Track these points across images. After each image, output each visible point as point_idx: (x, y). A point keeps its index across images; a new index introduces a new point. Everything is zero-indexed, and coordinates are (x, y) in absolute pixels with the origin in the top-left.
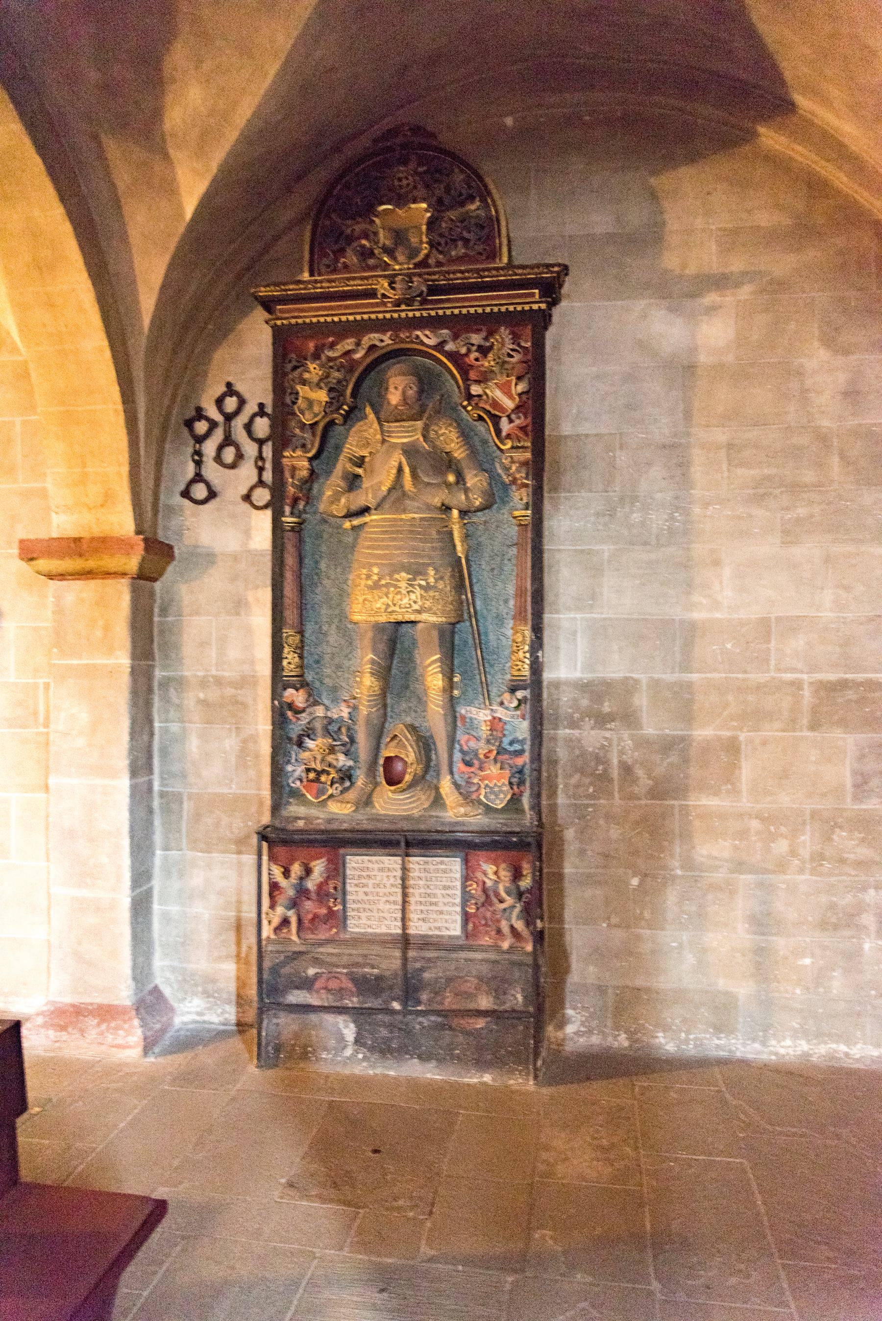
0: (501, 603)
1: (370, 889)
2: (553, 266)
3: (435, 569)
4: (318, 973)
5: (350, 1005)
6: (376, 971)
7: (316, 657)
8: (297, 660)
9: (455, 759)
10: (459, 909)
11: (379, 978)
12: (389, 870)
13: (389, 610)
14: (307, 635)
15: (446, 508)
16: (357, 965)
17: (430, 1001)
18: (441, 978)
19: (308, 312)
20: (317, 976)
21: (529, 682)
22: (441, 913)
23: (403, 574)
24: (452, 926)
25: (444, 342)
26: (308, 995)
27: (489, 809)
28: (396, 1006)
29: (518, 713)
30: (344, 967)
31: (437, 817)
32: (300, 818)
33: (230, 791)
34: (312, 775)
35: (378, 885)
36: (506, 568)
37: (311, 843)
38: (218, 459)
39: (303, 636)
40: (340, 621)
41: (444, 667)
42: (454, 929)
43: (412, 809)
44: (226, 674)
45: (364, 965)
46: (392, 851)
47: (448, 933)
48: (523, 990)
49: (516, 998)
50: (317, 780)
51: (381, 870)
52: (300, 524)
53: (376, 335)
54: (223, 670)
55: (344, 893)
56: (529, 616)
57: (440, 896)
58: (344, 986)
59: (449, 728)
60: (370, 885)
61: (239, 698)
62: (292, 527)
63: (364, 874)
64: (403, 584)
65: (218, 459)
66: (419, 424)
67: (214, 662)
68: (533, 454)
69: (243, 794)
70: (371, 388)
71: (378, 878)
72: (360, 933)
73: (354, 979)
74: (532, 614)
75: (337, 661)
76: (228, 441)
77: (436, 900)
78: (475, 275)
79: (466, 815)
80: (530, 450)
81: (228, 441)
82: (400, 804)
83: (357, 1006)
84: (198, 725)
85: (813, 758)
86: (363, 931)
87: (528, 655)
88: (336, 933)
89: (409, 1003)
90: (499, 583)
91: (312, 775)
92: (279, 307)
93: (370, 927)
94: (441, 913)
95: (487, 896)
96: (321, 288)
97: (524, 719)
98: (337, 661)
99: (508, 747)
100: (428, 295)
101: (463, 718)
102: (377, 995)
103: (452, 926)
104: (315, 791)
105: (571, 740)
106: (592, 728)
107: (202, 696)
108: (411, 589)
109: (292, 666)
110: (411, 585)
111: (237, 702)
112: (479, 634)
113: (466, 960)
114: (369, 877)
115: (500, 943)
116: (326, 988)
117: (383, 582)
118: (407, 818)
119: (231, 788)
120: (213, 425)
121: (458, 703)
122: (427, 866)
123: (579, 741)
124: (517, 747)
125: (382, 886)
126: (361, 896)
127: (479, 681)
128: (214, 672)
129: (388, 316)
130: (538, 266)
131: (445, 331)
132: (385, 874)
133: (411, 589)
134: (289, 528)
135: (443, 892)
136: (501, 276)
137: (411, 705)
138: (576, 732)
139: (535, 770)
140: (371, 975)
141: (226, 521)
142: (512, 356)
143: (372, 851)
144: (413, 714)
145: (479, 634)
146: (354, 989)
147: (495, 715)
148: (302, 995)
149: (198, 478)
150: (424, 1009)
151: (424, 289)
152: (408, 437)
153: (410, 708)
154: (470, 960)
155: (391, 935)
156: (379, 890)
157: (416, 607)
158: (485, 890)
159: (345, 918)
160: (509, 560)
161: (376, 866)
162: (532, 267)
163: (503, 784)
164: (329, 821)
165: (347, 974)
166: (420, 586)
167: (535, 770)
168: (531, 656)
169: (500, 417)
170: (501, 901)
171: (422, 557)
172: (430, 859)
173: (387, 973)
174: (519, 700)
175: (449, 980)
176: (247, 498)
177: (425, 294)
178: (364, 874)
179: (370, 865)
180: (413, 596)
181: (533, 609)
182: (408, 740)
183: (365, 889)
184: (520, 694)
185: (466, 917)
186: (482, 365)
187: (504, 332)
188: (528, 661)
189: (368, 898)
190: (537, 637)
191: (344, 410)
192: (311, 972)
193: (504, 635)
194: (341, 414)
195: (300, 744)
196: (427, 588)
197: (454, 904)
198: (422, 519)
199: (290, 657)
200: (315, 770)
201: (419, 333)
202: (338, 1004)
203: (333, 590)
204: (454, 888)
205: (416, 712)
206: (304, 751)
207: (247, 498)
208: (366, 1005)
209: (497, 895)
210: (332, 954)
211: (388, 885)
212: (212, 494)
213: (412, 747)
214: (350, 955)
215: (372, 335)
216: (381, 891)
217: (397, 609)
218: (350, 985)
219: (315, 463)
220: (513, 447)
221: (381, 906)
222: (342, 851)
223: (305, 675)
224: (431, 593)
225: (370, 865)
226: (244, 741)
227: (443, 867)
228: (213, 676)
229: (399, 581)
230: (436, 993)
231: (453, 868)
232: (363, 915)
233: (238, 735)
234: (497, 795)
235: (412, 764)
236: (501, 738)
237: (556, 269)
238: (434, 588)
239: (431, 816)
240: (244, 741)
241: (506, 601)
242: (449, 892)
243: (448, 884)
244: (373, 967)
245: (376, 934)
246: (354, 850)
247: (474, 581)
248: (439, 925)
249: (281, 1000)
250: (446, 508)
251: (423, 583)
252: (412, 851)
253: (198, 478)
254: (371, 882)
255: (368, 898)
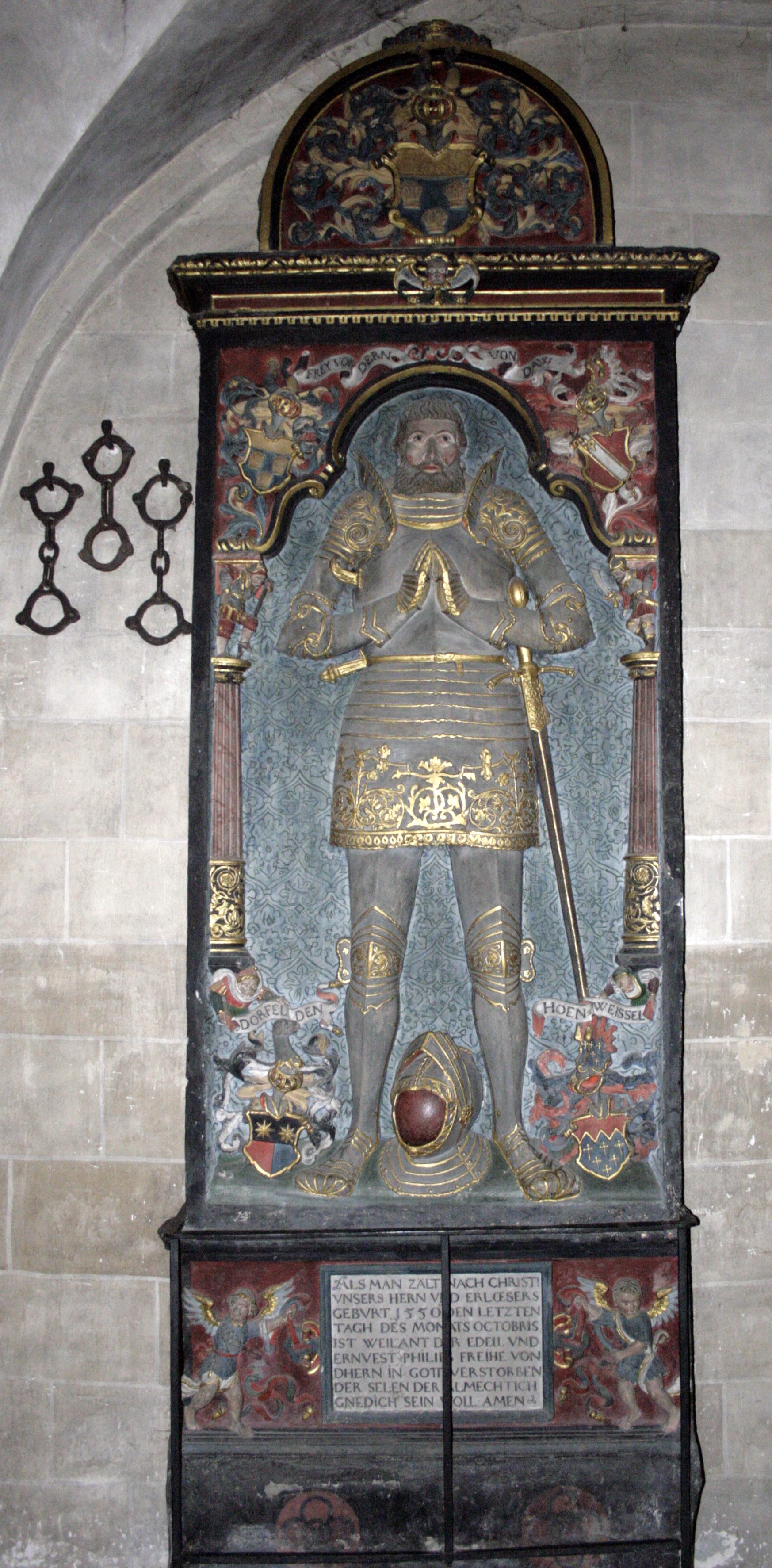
0: (606, 814)
1: (376, 1334)
2: (695, 252)
3: (491, 753)
4: (284, 1492)
5: (347, 1548)
6: (394, 1484)
7: (267, 910)
8: (234, 916)
9: (525, 1094)
10: (539, 1364)
11: (401, 1497)
12: (410, 1298)
13: (409, 826)
14: (250, 870)
15: (511, 645)
16: (358, 1474)
17: (497, 1534)
18: (516, 1490)
19: (265, 306)
20: (283, 1499)
21: (660, 953)
22: (508, 1372)
23: (435, 761)
24: (527, 1395)
25: (505, 367)
26: (268, 1534)
27: (593, 1184)
28: (433, 1545)
29: (642, 1008)
30: (334, 1478)
31: (498, 1200)
32: (243, 1209)
33: (97, 1159)
34: (264, 1128)
35: (391, 1327)
36: (613, 753)
37: (265, 1255)
38: (87, 555)
39: (243, 872)
40: (313, 845)
41: (508, 928)
42: (535, 1403)
43: (453, 1186)
44: (90, 943)
45: (372, 1475)
46: (421, 1264)
47: (519, 1407)
48: (664, 1502)
49: (652, 1518)
50: (274, 1136)
51: (397, 1299)
52: (241, 669)
53: (386, 349)
54: (84, 936)
55: (327, 1340)
56: (660, 836)
57: (504, 1341)
58: (337, 1513)
59: (517, 1038)
60: (376, 1327)
61: (115, 988)
62: (227, 674)
63: (365, 1307)
64: (435, 780)
65: (87, 555)
66: (460, 499)
67: (67, 920)
68: (661, 556)
69: (119, 1164)
70: (372, 438)
71: (392, 1313)
72: (354, 1415)
73: (351, 1498)
74: (666, 833)
75: (306, 917)
76: (107, 522)
77: (498, 1349)
78: (563, 259)
79: (553, 1195)
80: (656, 548)
81: (107, 522)
82: (429, 1178)
83: (361, 1549)
84: (34, 1037)
85: (384, 756)
86: (363, 1410)
87: (658, 906)
88: (314, 1415)
89: (456, 1539)
90: (602, 779)
91: (264, 1128)
92: (214, 297)
93: (377, 1402)
94: (508, 1372)
95: (592, 1338)
96: (295, 267)
97: (651, 1018)
98: (306, 917)
99: (620, 1071)
100: (479, 289)
101: (539, 1020)
102: (398, 1526)
103: (527, 1395)
104: (268, 1157)
105: (718, 1056)
106: (753, 1034)
107: (42, 982)
108: (449, 787)
109: (226, 928)
110: (448, 780)
111: (108, 995)
112: (567, 872)
113: (559, 1455)
114: (374, 1312)
115: (614, 1420)
116: (301, 1519)
117: (398, 775)
118: (440, 1204)
119: (97, 1152)
120: (75, 491)
121: (529, 993)
122: (480, 1290)
123: (732, 1056)
124: (638, 1069)
125: (398, 1328)
126: (359, 1347)
127: (567, 952)
128: (66, 940)
129: (409, 318)
130: (669, 251)
131: (507, 348)
132: (402, 1307)
133: (449, 787)
134: (223, 677)
135: (513, 1335)
136: (606, 263)
137: (444, 997)
138: (727, 1040)
139: (674, 1109)
140: (386, 1490)
141: (95, 665)
142: (624, 394)
143: (379, 1266)
144: (449, 1015)
145: (567, 872)
146: (354, 1518)
147: (598, 1013)
148: (255, 1534)
149: (47, 587)
150: (484, 1547)
151: (475, 278)
152: (441, 521)
153: (442, 1002)
154: (566, 1455)
155: (415, 1415)
156: (390, 1335)
157: (459, 820)
158: (588, 1328)
159: (330, 1389)
160: (620, 738)
161: (386, 1292)
162: (660, 252)
163: (617, 1138)
164: (297, 1212)
165: (341, 1491)
166: (465, 781)
167: (674, 1109)
168: (663, 907)
169: (606, 493)
170: (624, 1346)
171: (464, 729)
172: (487, 1277)
173: (415, 1487)
174: (643, 986)
175: (530, 1493)
176: (134, 623)
177: (475, 285)
178: (365, 1307)
179: (375, 1291)
180: (453, 801)
181: (666, 823)
182: (443, 1060)
183: (367, 1335)
184: (646, 975)
185: (553, 1378)
186: (570, 406)
187: (609, 355)
188: (658, 917)
189: (371, 1350)
190: (674, 873)
191: (326, 472)
192: (273, 1490)
193: (610, 870)
194: (321, 480)
195: (237, 1069)
196: (477, 786)
197: (530, 1356)
198: (464, 664)
199: (222, 910)
200: (269, 1119)
201: (458, 348)
202: (326, 1548)
203: (300, 789)
204: (530, 1326)
205: (452, 1009)
206: (247, 1084)
207: (134, 623)
208: (376, 1548)
209: (610, 1334)
210: (309, 1456)
211: (409, 1326)
212: (71, 615)
213: (452, 1075)
214: (344, 1456)
215: (379, 350)
216: (397, 1337)
217: (424, 823)
218: (348, 1512)
219: (269, 563)
220: (626, 544)
221: (396, 1365)
222: (323, 1266)
223: (248, 944)
224: (486, 795)
225: (375, 1291)
226: (123, 1066)
227: (511, 1289)
228: (65, 947)
229: (427, 773)
230: (505, 1517)
231: (530, 1291)
232: (363, 1383)
233: (109, 1055)
234: (605, 1157)
235: (451, 1104)
236: (610, 1053)
237: (698, 258)
238: (491, 786)
239: (486, 1199)
240: (123, 1066)
241: (614, 811)
242: (525, 1334)
243: (518, 1320)
244: (387, 1476)
245: (385, 1417)
246: (345, 1265)
247: (557, 774)
248: (505, 1393)
249: (218, 1544)
250: (511, 645)
251: (471, 776)
252: (456, 1263)
253: (47, 587)
254: (377, 1322)
255: (371, 1350)
